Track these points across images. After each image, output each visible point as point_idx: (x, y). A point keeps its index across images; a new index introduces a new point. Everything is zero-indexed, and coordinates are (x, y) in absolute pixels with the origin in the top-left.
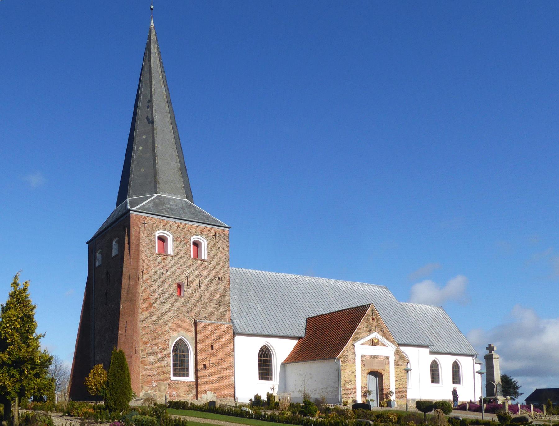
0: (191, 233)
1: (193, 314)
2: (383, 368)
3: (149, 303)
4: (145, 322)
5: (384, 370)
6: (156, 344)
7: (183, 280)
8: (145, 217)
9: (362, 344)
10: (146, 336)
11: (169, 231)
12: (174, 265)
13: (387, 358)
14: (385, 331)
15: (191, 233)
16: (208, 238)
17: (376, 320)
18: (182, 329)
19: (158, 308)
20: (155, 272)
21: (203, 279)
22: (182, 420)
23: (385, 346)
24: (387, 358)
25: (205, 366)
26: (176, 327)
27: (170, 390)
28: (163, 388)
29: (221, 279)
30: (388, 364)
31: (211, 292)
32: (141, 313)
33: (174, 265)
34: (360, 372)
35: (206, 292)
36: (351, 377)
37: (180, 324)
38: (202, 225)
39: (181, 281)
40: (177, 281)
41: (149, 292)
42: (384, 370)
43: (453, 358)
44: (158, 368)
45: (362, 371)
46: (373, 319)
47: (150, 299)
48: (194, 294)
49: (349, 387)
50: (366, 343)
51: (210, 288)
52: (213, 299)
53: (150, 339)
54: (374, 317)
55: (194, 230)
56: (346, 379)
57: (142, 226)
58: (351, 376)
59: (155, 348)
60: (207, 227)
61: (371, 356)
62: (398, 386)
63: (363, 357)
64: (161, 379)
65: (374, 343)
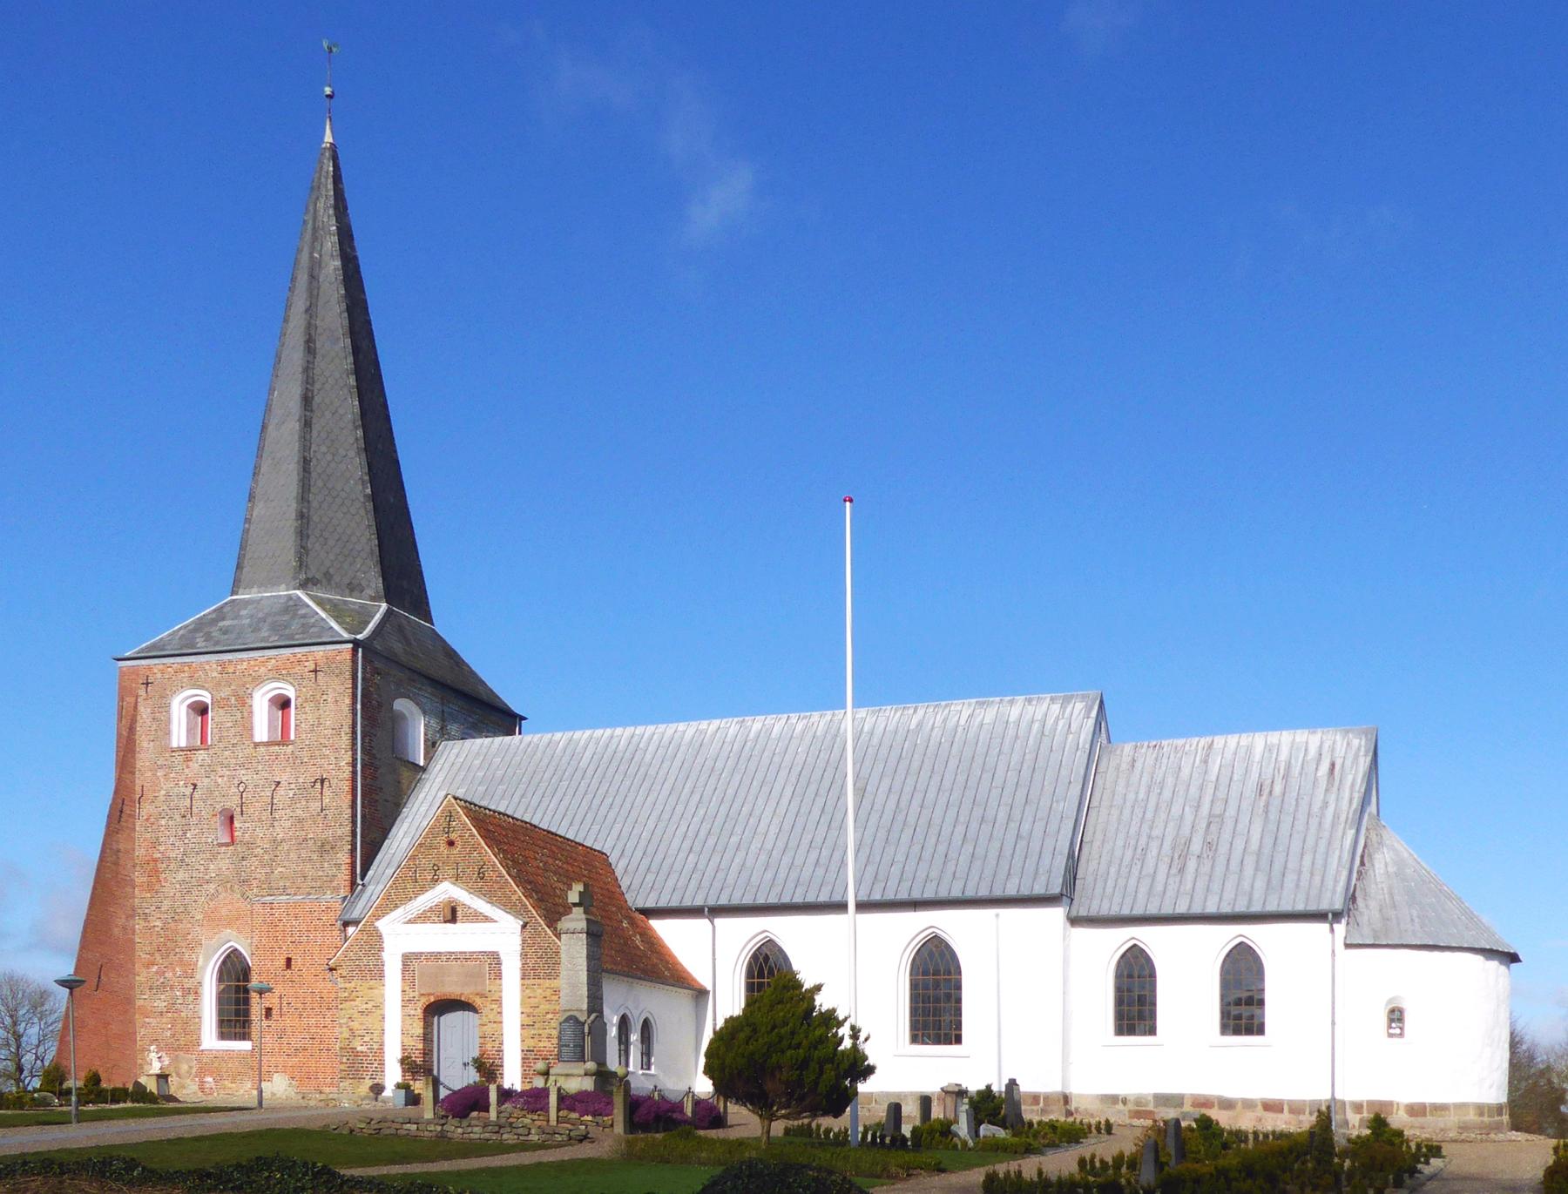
0: (254, 679)
1: (255, 883)
2: (479, 989)
3: (154, 869)
4: (146, 917)
5: (483, 996)
6: (171, 966)
7: (232, 803)
8: (149, 668)
9: (410, 922)
10: (148, 949)
11: (202, 687)
12: (210, 770)
13: (494, 959)
14: (489, 874)
15: (254, 679)
16: (298, 681)
17: (459, 844)
18: (229, 925)
19: (174, 879)
20: (168, 795)
21: (281, 791)
22: (1001, 1175)
23: (487, 919)
24: (494, 959)
25: (269, 1011)
26: (215, 921)
27: (202, 1071)
28: (185, 1067)
29: (326, 784)
30: (499, 976)
31: (300, 820)
32: (140, 897)
33: (210, 770)
34: (399, 1003)
35: (288, 824)
36: (369, 1021)
37: (224, 912)
38: (282, 651)
39: (228, 805)
40: (219, 807)
41: (155, 844)
42: (483, 996)
43: (1223, 937)
44: (173, 1022)
45: (407, 1002)
46: (451, 843)
47: (155, 861)
48: (259, 833)
49: (364, 1049)
50: (422, 918)
51: (299, 812)
52: (305, 840)
53: (157, 955)
54: (453, 836)
55: (263, 669)
56: (355, 1025)
57: (142, 692)
58: (370, 1019)
59: (169, 975)
60: (294, 655)
61: (437, 956)
62: (531, 1043)
63: (408, 959)
64: (179, 1048)
65: (452, 914)
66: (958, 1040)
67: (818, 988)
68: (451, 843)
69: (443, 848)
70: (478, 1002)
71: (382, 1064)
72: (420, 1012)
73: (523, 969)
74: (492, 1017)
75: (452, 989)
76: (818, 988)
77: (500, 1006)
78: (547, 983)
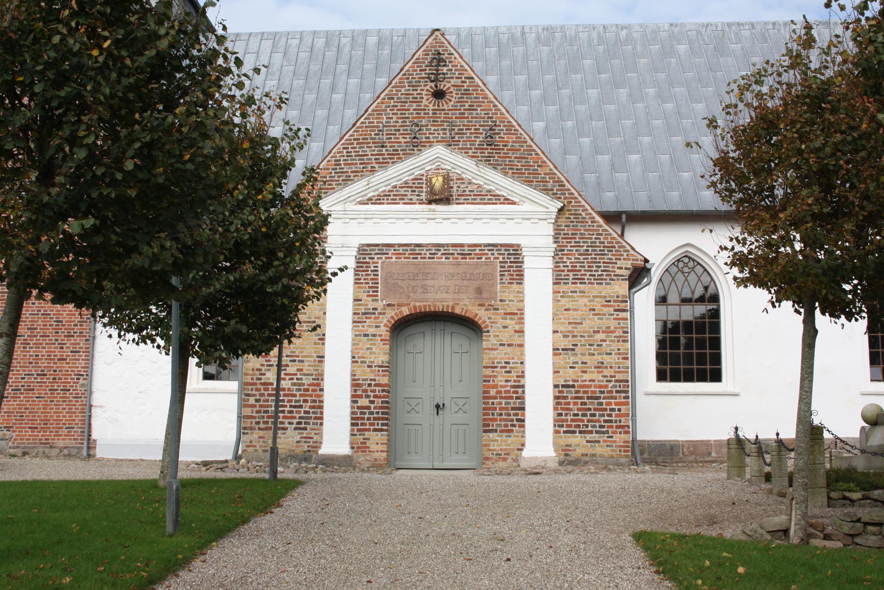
13: (512, 257)
23: (496, 198)
24: (512, 257)
30: (519, 277)
34: (349, 317)
45: (360, 316)
46: (439, 95)
54: (444, 86)
62: (569, 375)
63: (366, 253)
66: (716, 377)
67: (757, 436)
68: (439, 95)
69: (427, 102)
70: (482, 315)
71: (319, 406)
72: (384, 331)
73: (557, 270)
74: (505, 337)
75: (439, 298)
76: (757, 436)
77: (521, 321)
78: (596, 289)
